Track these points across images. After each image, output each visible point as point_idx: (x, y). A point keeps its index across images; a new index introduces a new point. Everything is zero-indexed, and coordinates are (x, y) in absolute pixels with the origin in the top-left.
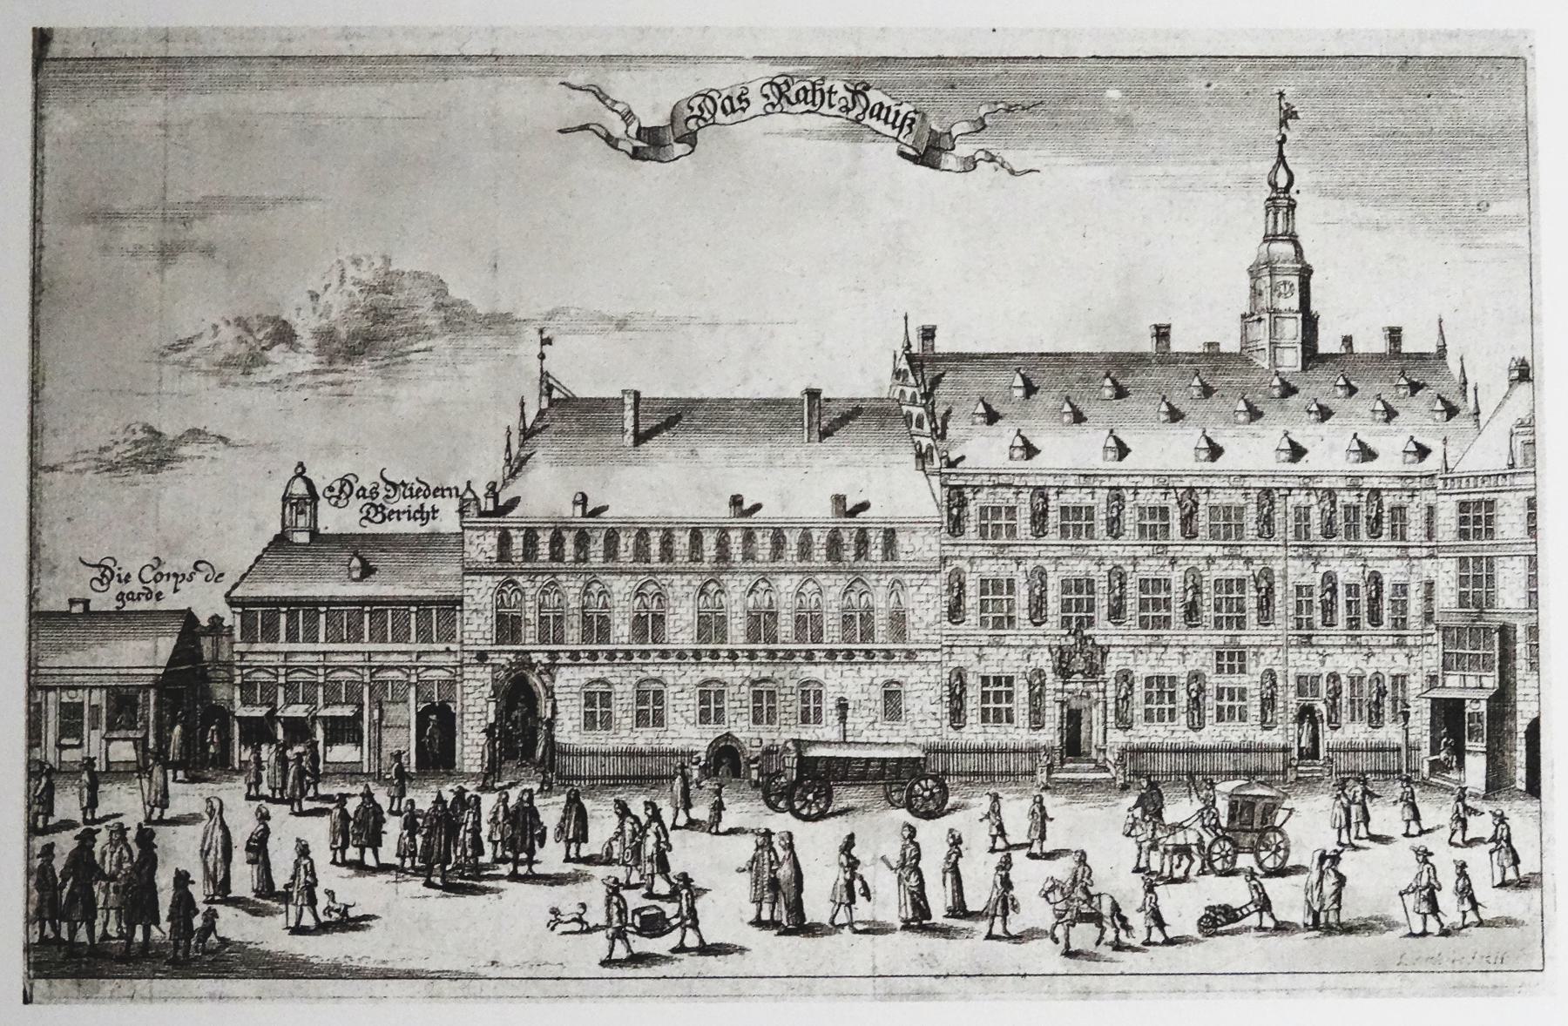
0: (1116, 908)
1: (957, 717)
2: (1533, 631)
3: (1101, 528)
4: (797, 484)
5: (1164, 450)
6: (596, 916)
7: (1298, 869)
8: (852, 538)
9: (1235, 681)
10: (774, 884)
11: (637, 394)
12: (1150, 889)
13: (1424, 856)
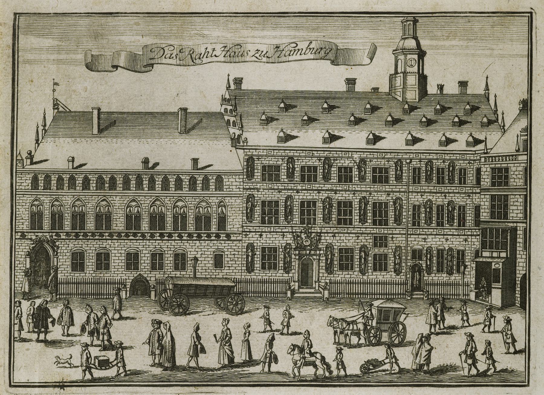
0: (323, 358)
1: (250, 268)
2: (527, 233)
3: (320, 176)
4: (175, 153)
5: (355, 139)
6: (76, 361)
7: (410, 343)
8: (200, 178)
9: (382, 250)
10: (162, 347)
11: (99, 109)
12: (340, 351)
13: (471, 336)
